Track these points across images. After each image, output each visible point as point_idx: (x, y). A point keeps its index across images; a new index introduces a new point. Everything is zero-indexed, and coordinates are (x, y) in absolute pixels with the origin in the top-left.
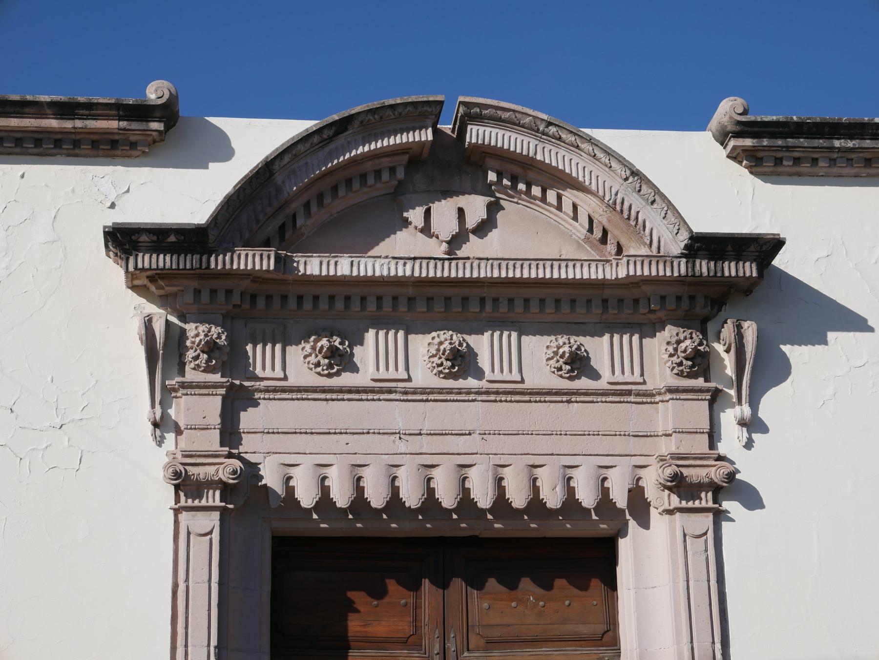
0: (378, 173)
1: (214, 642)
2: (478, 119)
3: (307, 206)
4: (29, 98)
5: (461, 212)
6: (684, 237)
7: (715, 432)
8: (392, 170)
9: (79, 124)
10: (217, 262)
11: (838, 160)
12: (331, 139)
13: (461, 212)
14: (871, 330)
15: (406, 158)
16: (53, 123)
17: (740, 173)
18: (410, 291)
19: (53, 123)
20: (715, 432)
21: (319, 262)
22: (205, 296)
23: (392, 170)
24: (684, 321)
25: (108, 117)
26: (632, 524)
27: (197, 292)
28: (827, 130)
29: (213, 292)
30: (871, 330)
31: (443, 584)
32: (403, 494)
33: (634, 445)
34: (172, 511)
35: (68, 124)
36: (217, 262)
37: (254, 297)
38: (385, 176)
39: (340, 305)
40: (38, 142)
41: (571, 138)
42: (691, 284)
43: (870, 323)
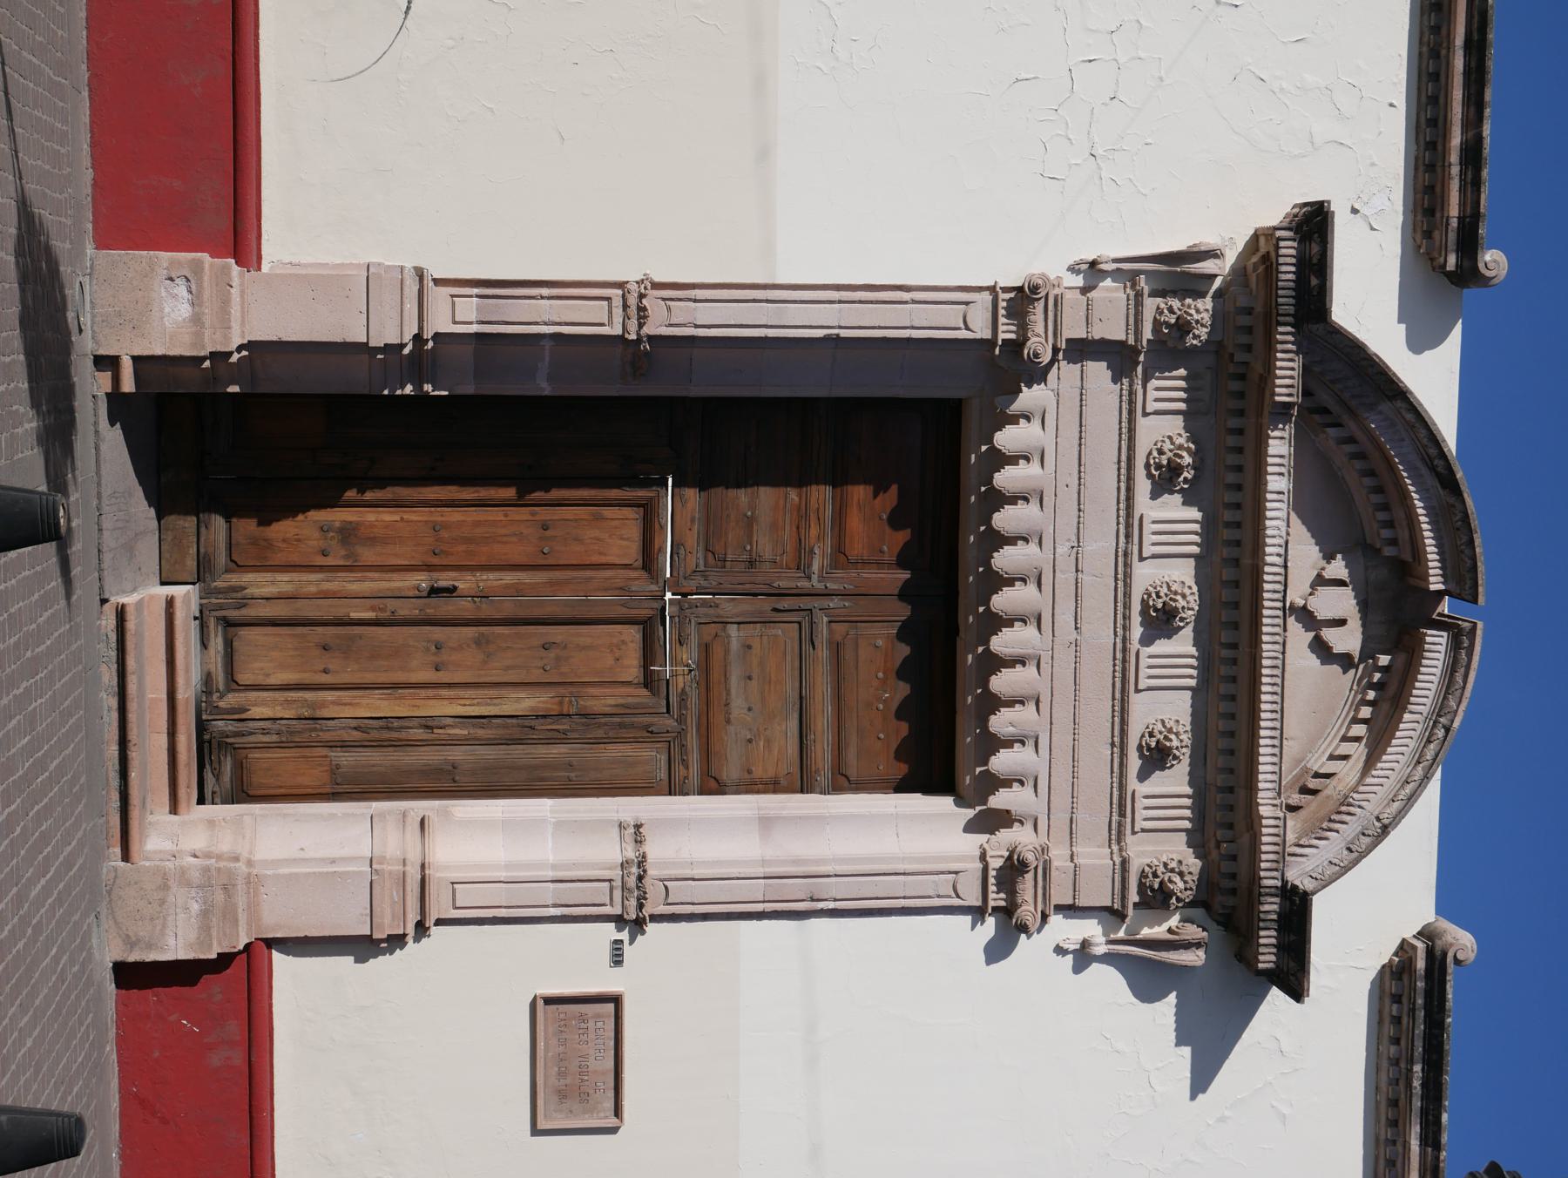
0: (1390, 524)
1: (844, 333)
2: (1455, 645)
4: (1487, 112)
5: (1341, 622)
6: (1306, 884)
8: (1393, 542)
9: (1455, 170)
10: (1285, 335)
13: (1341, 622)
15: (1408, 557)
16: (1456, 140)
18: (1246, 561)
19: (1456, 140)
22: (1244, 320)
23: (1393, 542)
24: (1207, 882)
25: (1462, 204)
26: (970, 813)
27: (1249, 311)
28: (1434, 1057)
29: (1249, 330)
30: (1193, 1097)
31: (905, 594)
33: (1059, 819)
35: (1454, 157)
36: (1285, 335)
37: (1242, 377)
38: (1386, 533)
40: (1433, 122)
41: (1429, 755)
42: (1250, 892)
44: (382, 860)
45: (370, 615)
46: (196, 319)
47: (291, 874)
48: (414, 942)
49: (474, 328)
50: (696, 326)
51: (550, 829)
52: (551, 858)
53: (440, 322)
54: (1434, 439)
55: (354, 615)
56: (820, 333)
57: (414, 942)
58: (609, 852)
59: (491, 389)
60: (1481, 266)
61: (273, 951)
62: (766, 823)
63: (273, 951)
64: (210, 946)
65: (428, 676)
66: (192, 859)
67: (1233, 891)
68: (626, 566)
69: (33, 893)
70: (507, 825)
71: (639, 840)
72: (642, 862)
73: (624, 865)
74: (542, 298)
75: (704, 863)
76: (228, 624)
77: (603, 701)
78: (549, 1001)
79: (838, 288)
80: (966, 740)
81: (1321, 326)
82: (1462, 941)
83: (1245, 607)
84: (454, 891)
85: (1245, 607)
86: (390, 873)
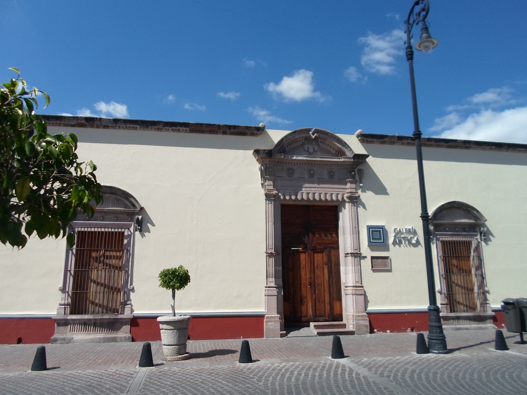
0: (300, 141)
1: (273, 222)
3: (288, 146)
6: (353, 154)
7: (345, 214)
8: (302, 140)
11: (424, 22)
12: (293, 134)
14: (387, 194)
15: (304, 138)
17: (187, 286)
18: (305, 162)
20: (345, 214)
21: (313, 148)
22: (270, 162)
23: (302, 140)
27: (269, 161)
29: (272, 161)
32: (304, 197)
33: (342, 190)
34: (265, 200)
37: (278, 162)
38: (301, 141)
39: (293, 164)
43: (388, 191)
44: (353, 293)
45: (314, 295)
46: (275, 321)
47: (356, 307)
48: (176, 268)
49: (274, 279)
50: (273, 245)
51: (346, 267)
52: (351, 267)
53: (273, 285)
54: (289, 135)
55: (314, 297)
56: (273, 226)
57: (176, 268)
58: (350, 259)
59: (281, 277)
60: (262, 127)
61: (367, 309)
62: (344, 234)
63: (367, 309)
64: (367, 319)
65: (322, 286)
66: (354, 322)
67: (353, 165)
68: (305, 255)
69: (437, 352)
70: (346, 274)
71: (348, 254)
72: (351, 254)
73: (352, 256)
74: (269, 268)
75: (351, 243)
76: (316, 317)
77: (325, 259)
78: (372, 267)
79: (266, 223)
80: (325, 204)
81: (273, 151)
82: (359, 131)
83: (312, 162)
84: (357, 282)
85: (312, 162)
86: (355, 291)
